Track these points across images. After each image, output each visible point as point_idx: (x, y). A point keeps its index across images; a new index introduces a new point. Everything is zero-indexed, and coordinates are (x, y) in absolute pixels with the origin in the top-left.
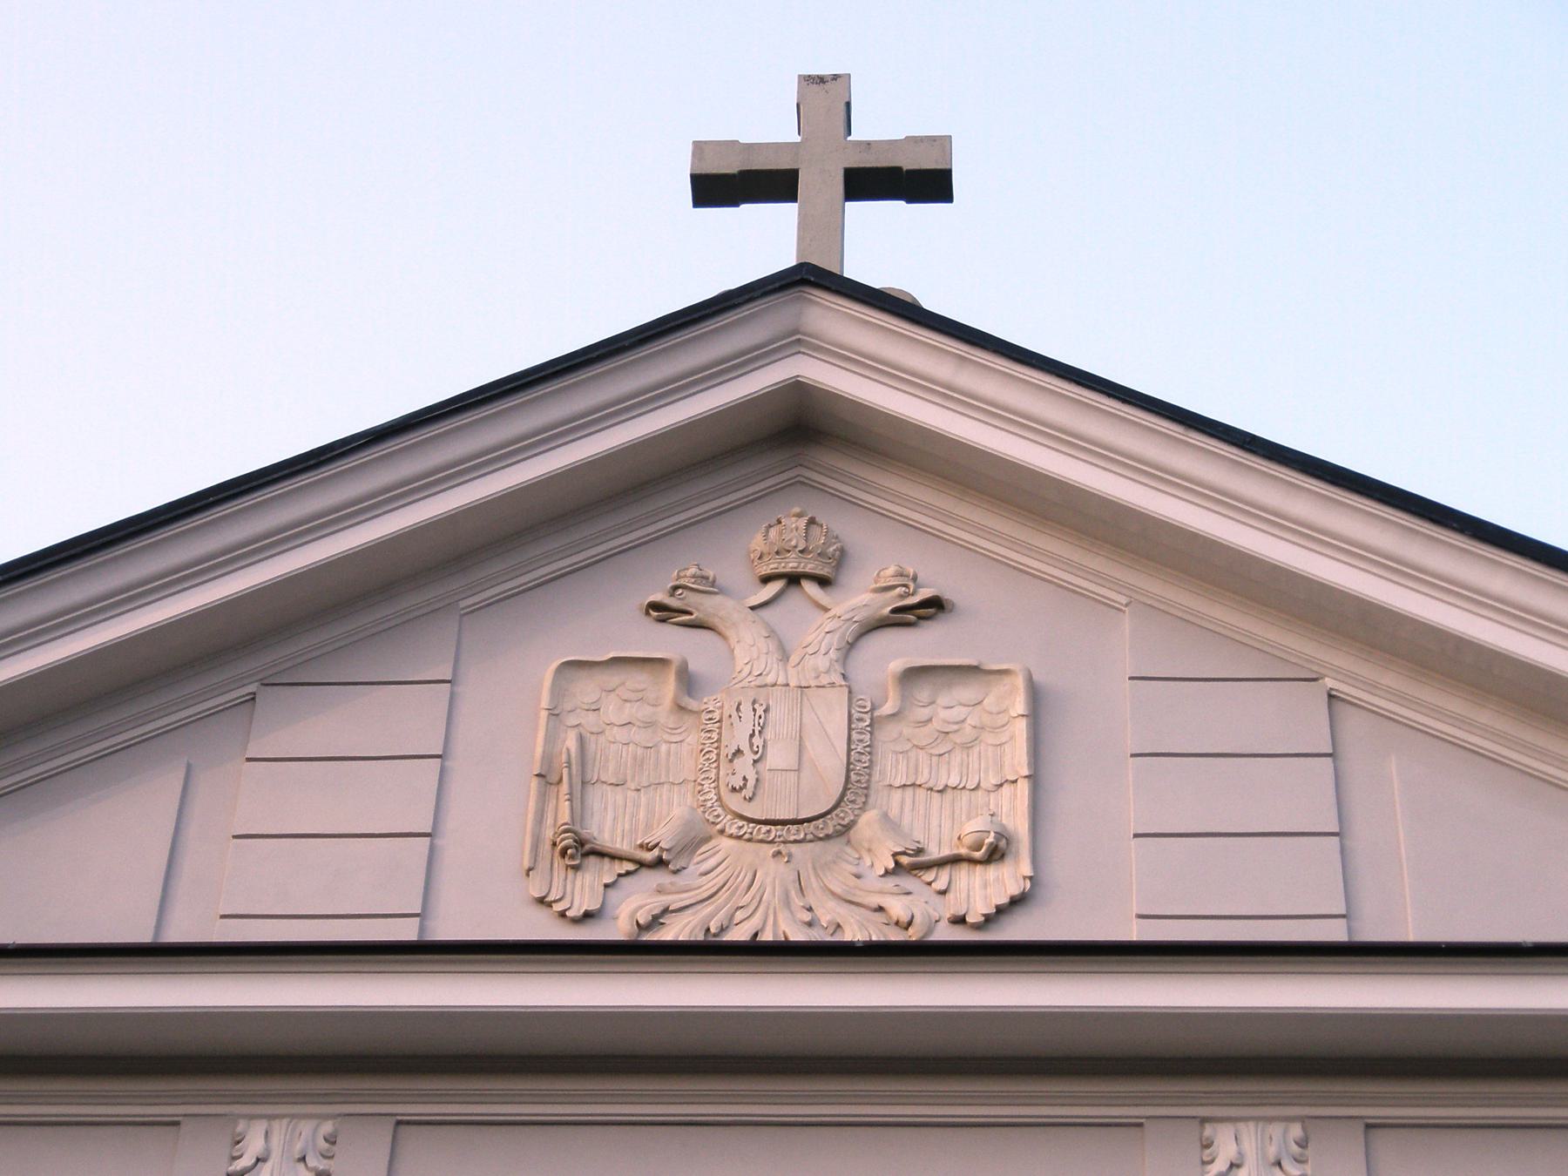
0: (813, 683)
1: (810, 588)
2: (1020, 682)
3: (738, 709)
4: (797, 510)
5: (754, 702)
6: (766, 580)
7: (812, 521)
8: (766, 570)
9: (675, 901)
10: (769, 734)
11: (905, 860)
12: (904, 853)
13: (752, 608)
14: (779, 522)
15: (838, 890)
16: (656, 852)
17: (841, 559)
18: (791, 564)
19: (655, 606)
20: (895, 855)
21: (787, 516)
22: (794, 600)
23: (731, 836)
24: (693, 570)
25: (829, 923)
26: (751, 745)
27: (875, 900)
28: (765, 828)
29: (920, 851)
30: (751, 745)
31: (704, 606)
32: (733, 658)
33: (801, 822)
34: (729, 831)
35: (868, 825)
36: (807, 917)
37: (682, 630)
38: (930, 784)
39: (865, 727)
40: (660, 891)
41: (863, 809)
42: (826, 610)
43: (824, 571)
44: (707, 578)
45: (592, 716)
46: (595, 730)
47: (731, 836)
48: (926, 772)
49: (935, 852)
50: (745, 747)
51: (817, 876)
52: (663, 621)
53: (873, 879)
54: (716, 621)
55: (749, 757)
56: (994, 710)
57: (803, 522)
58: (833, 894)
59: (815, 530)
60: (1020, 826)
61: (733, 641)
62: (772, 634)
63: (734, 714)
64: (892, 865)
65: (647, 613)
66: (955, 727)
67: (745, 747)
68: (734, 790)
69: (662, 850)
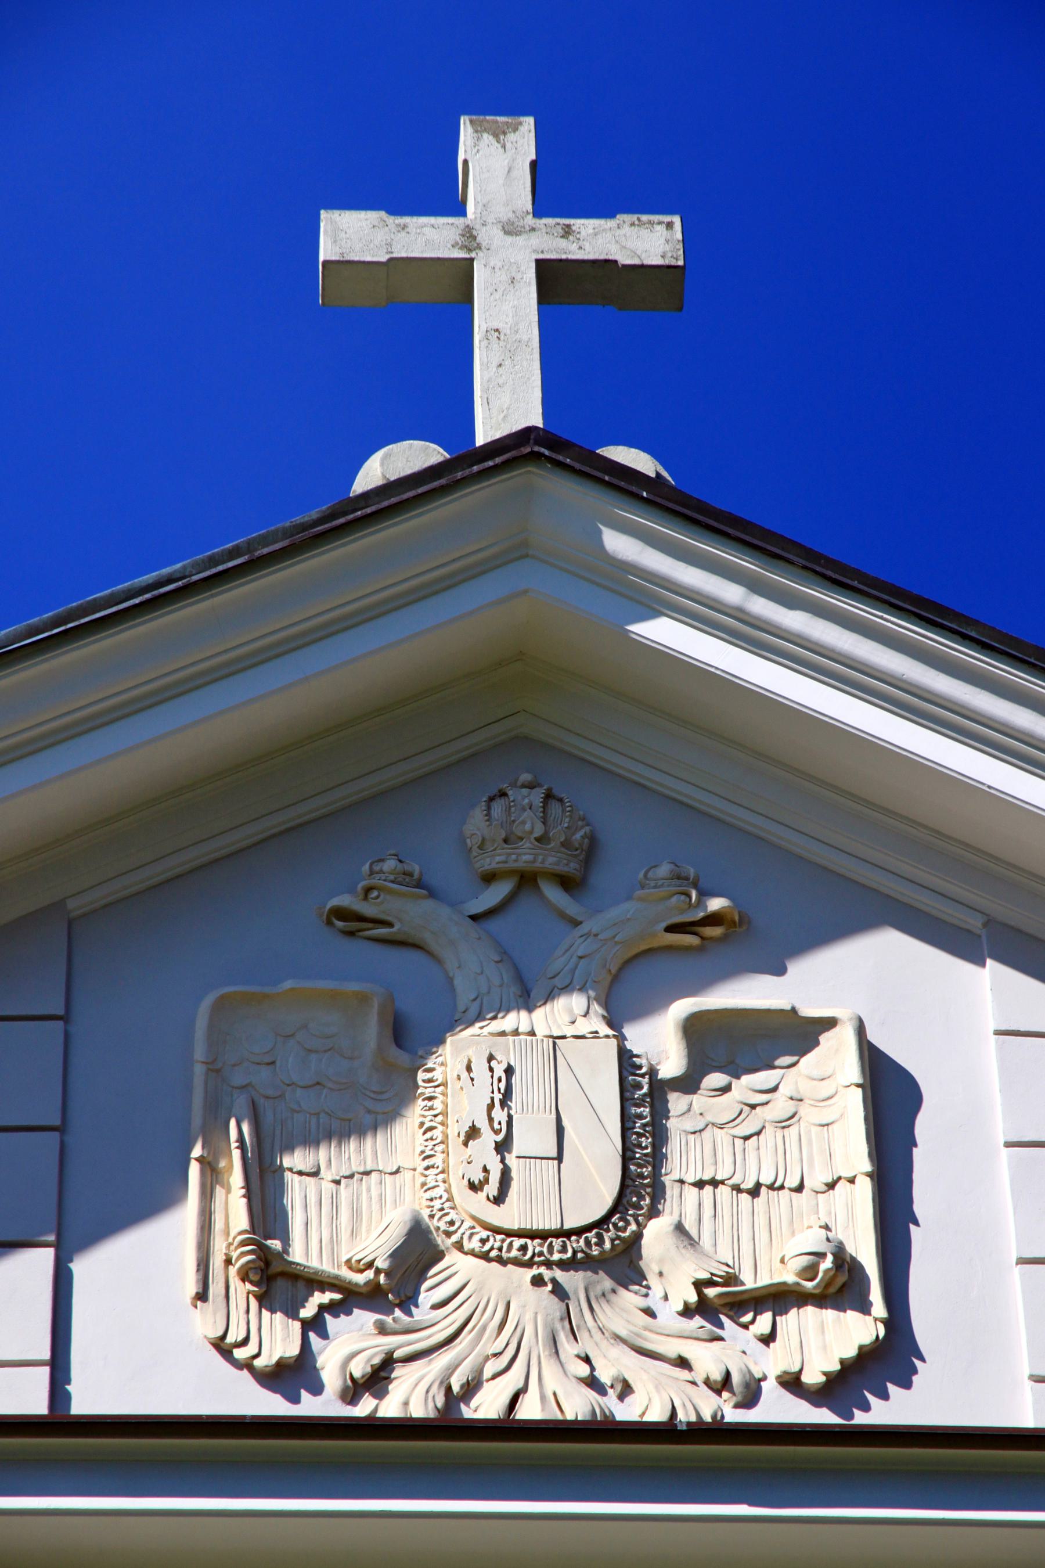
0: (569, 1031)
1: (553, 893)
2: (837, 1061)
3: (469, 1069)
4: (526, 777)
5: (491, 1058)
6: (489, 878)
7: (549, 796)
8: (490, 863)
9: (402, 1344)
10: (515, 1103)
11: (711, 1292)
12: (711, 1283)
13: (474, 918)
14: (503, 794)
15: (623, 1333)
16: (370, 1274)
17: (590, 851)
18: (525, 857)
19: (340, 913)
20: (699, 1285)
21: (513, 785)
22: (527, 906)
23: (472, 1253)
24: (390, 864)
25: (616, 1379)
26: (491, 1120)
27: (672, 1348)
28: (518, 1243)
29: (731, 1279)
30: (491, 1120)
31: (410, 913)
32: (453, 989)
33: (568, 1234)
34: (467, 1246)
35: (656, 1236)
36: (584, 1370)
37: (366, 942)
38: (735, 1181)
39: (645, 1103)
40: (382, 1330)
41: (654, 1212)
42: (576, 923)
43: (571, 868)
44: (411, 875)
45: (265, 1073)
46: (270, 1092)
47: (472, 1253)
48: (729, 1160)
49: (753, 1280)
50: (483, 1124)
51: (591, 1309)
52: (351, 934)
53: (668, 1314)
54: (428, 939)
55: (488, 1139)
56: (816, 1073)
57: (537, 797)
58: (617, 1337)
59: (555, 808)
60: (865, 1251)
61: (451, 964)
62: (505, 956)
63: (465, 1075)
64: (693, 1298)
65: (329, 923)
66: (764, 1097)
67: (483, 1124)
68: (473, 1187)
69: (378, 1271)
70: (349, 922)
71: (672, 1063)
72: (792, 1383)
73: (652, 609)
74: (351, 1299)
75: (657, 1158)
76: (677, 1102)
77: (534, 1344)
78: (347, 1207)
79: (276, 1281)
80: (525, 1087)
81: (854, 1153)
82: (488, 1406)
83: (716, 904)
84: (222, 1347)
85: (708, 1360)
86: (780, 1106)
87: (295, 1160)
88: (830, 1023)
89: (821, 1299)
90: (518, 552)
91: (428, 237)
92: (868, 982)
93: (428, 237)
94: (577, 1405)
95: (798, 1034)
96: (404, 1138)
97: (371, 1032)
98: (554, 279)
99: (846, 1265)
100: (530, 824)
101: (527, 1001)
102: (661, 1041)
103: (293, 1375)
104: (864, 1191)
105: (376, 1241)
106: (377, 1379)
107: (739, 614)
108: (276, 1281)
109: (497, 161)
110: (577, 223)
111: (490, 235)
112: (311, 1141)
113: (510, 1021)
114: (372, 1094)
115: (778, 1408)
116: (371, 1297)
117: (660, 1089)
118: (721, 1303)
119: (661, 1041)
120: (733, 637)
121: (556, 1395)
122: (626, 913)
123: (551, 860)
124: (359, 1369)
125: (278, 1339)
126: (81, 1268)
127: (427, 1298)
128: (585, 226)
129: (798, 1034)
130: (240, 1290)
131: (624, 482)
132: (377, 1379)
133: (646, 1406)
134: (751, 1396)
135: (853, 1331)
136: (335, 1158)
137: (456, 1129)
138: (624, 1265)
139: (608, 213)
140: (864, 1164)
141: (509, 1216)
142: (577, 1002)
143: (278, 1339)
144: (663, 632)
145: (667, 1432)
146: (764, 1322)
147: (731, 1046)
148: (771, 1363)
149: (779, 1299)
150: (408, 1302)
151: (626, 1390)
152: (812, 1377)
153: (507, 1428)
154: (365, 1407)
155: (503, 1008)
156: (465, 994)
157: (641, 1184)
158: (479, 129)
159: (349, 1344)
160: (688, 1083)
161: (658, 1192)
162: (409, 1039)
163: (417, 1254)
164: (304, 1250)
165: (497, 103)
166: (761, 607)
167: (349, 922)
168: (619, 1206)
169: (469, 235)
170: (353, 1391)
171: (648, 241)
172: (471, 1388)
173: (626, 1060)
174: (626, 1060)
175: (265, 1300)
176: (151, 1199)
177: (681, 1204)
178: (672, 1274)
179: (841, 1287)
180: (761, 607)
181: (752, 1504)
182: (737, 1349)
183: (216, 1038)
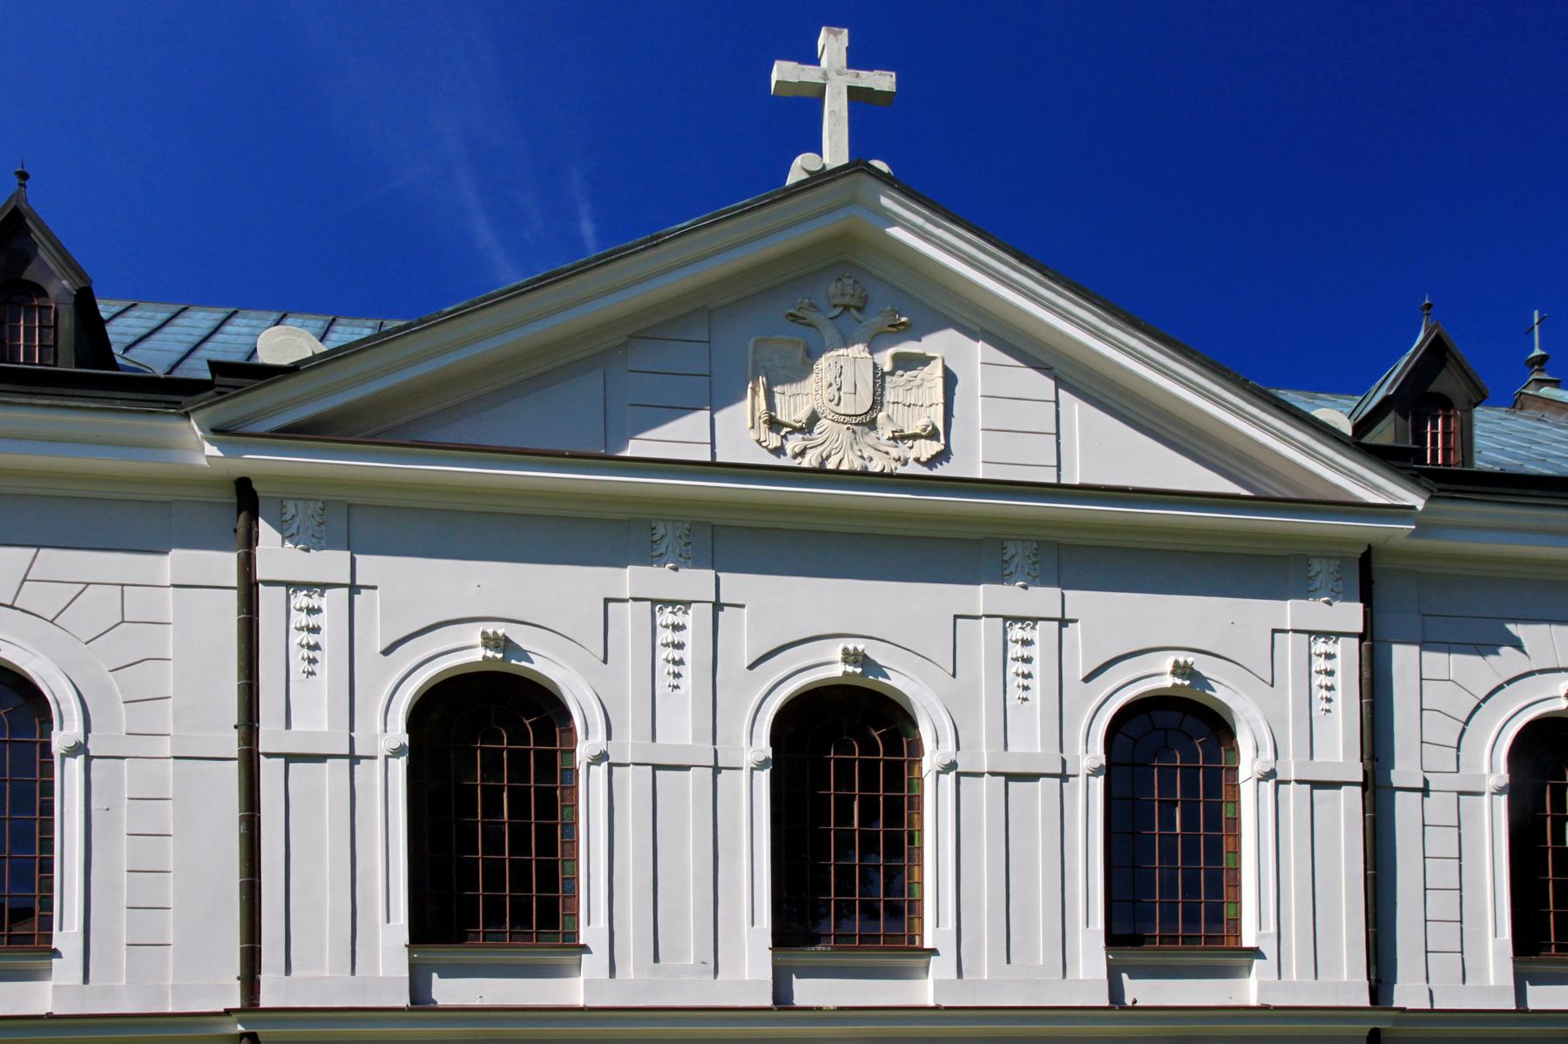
1: (854, 312)
2: (936, 370)
6: (835, 306)
8: (835, 302)
17: (865, 299)
18: (847, 300)
19: (791, 315)
27: (885, 449)
31: (811, 316)
39: (880, 377)
55: (835, 387)
62: (840, 332)
70: (794, 318)
71: (887, 367)
72: (917, 460)
73: (893, 223)
74: (795, 430)
75: (882, 395)
76: (888, 378)
77: (846, 444)
78: (794, 403)
79: (774, 424)
80: (842, 372)
81: (939, 396)
82: (831, 465)
83: (904, 319)
84: (758, 442)
85: (894, 453)
86: (918, 381)
87: (777, 389)
88: (934, 358)
89: (926, 437)
90: (853, 202)
91: (808, 74)
92: (943, 345)
93: (808, 74)
94: (857, 465)
95: (924, 360)
96: (810, 383)
97: (800, 353)
98: (853, 92)
99: (935, 429)
100: (849, 290)
101: (846, 346)
102: (885, 359)
103: (779, 451)
104: (940, 408)
105: (801, 415)
106: (802, 453)
107: (921, 228)
108: (774, 424)
109: (833, 44)
110: (862, 73)
111: (832, 75)
112: (783, 383)
113: (842, 351)
114: (800, 370)
115: (914, 469)
116: (801, 430)
117: (884, 374)
118: (899, 437)
119: (885, 359)
120: (921, 236)
121: (850, 462)
122: (875, 321)
123: (854, 302)
124: (797, 450)
125: (774, 441)
126: (717, 416)
127: (816, 431)
128: (863, 73)
129: (924, 360)
130: (764, 427)
131: (878, 174)
132: (802, 453)
133: (875, 467)
134: (905, 463)
135: (935, 447)
136: (789, 389)
137: (825, 384)
138: (872, 425)
139: (871, 69)
140: (941, 400)
141: (841, 409)
142: (861, 346)
143: (774, 441)
144: (896, 232)
145: (881, 474)
146: (910, 443)
147: (905, 363)
148: (912, 455)
149: (915, 437)
150: (811, 432)
151: (871, 460)
152: (923, 459)
153: (837, 472)
154: (795, 463)
155: (840, 347)
156: (827, 343)
157: (877, 404)
158: (829, 32)
159: (794, 443)
160: (892, 373)
161: (882, 404)
162: (812, 355)
163: (814, 419)
164: (781, 416)
165: (835, 22)
166: (929, 227)
167: (794, 318)
168: (872, 408)
169: (825, 75)
170: (795, 456)
171: (883, 81)
172: (828, 457)
173: (875, 366)
174: (875, 366)
175: (771, 429)
176: (738, 397)
177: (889, 408)
178: (885, 431)
179: (933, 435)
180: (929, 227)
181: (1403, 353)
182: (901, 450)
183: (755, 351)
